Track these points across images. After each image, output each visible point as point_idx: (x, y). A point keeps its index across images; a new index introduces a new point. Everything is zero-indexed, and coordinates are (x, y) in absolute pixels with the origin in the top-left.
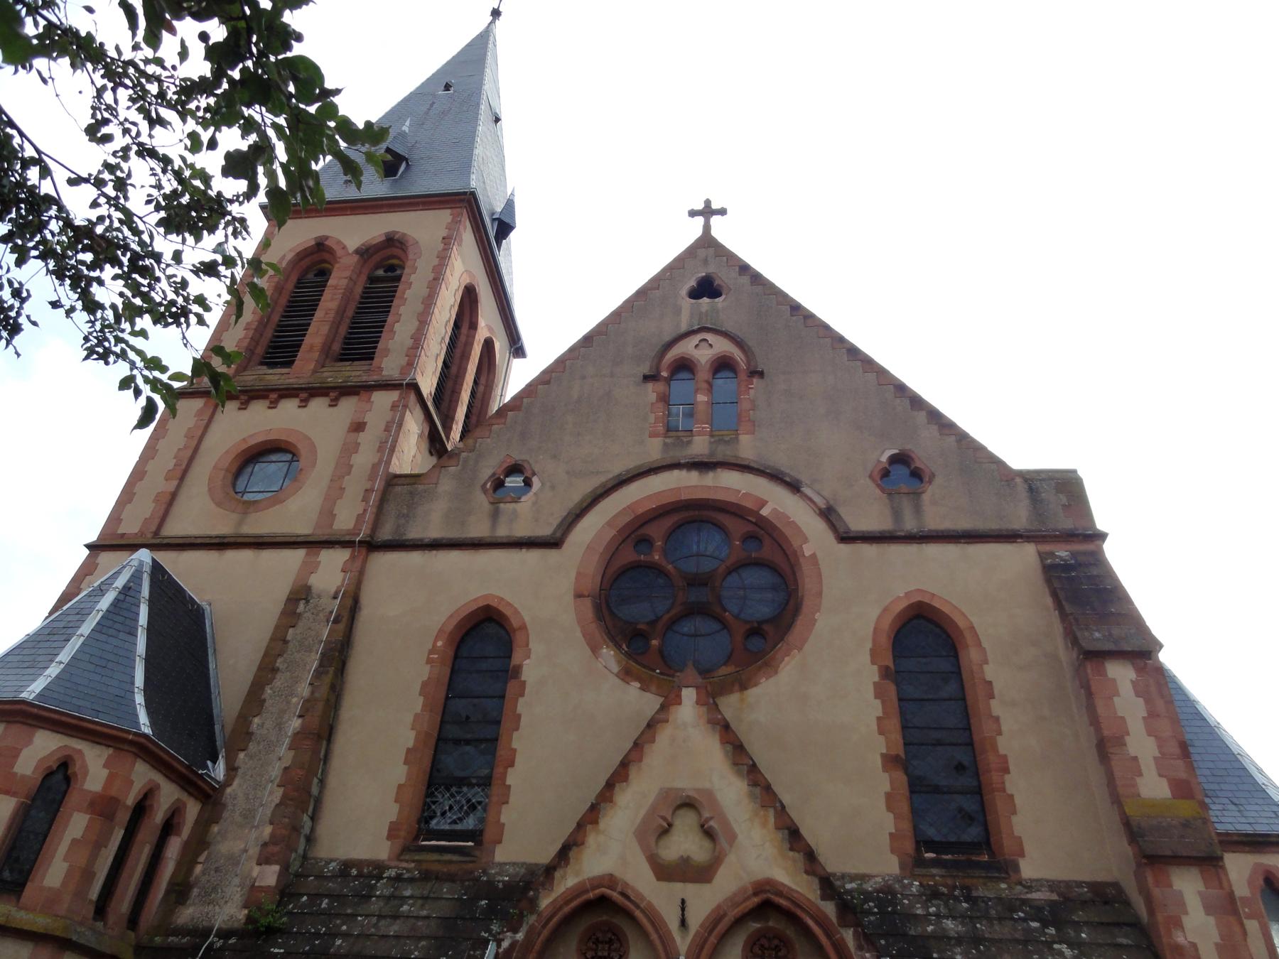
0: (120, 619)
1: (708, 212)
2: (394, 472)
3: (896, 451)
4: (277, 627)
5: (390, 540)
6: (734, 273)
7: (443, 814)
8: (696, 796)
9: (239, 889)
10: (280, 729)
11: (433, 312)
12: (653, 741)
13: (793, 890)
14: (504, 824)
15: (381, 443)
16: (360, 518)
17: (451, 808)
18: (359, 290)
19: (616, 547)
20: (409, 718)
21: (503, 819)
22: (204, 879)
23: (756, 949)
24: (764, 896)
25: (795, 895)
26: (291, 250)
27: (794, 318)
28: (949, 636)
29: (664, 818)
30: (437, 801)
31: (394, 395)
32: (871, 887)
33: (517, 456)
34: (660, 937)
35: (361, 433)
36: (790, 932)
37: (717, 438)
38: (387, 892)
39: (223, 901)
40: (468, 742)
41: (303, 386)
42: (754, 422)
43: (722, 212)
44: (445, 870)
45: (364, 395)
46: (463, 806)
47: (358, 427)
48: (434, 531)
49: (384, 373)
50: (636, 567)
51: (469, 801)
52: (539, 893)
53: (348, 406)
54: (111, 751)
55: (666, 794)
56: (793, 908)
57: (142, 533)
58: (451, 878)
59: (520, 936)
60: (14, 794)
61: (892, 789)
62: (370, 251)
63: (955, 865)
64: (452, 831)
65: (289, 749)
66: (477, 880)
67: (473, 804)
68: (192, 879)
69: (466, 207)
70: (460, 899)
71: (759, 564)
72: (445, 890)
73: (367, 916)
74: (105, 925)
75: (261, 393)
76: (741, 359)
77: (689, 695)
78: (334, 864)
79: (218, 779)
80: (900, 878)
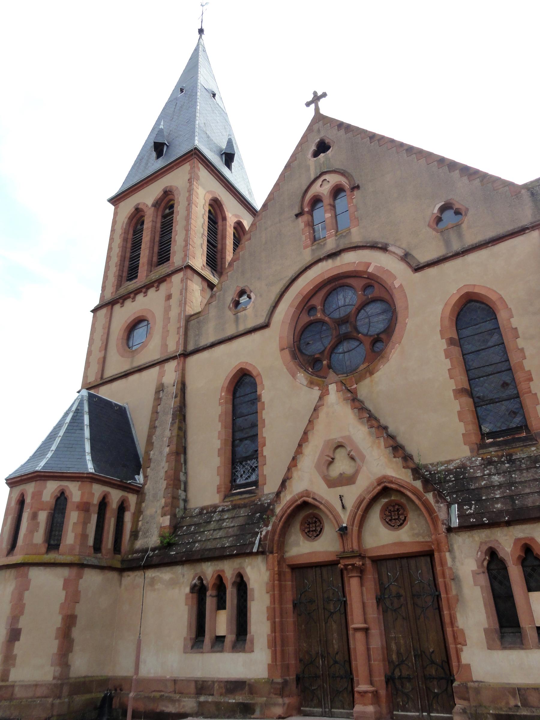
0: (76, 424)
1: (316, 98)
2: (190, 314)
3: (443, 203)
4: (153, 407)
5: (193, 349)
6: (335, 131)
7: (241, 476)
8: (342, 441)
9: (156, 529)
10: (162, 454)
11: (191, 223)
12: (318, 417)
13: (398, 479)
14: (266, 475)
15: (180, 302)
16: (178, 343)
17: (244, 472)
18: (159, 225)
19: (297, 317)
20: (216, 434)
21: (265, 473)
22: (143, 528)
23: (387, 513)
24: (383, 485)
25: (399, 481)
26: (125, 218)
27: (373, 144)
28: (490, 308)
29: (328, 456)
30: (238, 471)
31: (180, 275)
32: (453, 466)
33: (241, 285)
34: (334, 517)
35: (171, 300)
36: (403, 501)
37: (339, 236)
38: (217, 518)
39: (151, 535)
40: (246, 439)
41: (142, 286)
42: (358, 218)
43: (324, 95)
44: (243, 503)
45: (168, 280)
46: (249, 470)
47: (169, 297)
48: (212, 339)
49: (176, 265)
50: (310, 324)
51: (251, 467)
52: (275, 506)
53: (163, 287)
54: (80, 483)
55: (327, 443)
56: (399, 488)
57: (96, 380)
58: (245, 506)
59: (270, 528)
60: (45, 510)
61: (461, 408)
62: (159, 203)
63: (505, 443)
64: (247, 483)
65: (166, 462)
66: (256, 504)
67: (253, 468)
68: (139, 528)
69: (195, 157)
70: (248, 515)
71: (374, 300)
72: (242, 512)
73: (209, 531)
74: (102, 555)
75: (126, 296)
76: (345, 183)
77: (332, 388)
78: (197, 510)
79: (141, 483)
80: (470, 458)
